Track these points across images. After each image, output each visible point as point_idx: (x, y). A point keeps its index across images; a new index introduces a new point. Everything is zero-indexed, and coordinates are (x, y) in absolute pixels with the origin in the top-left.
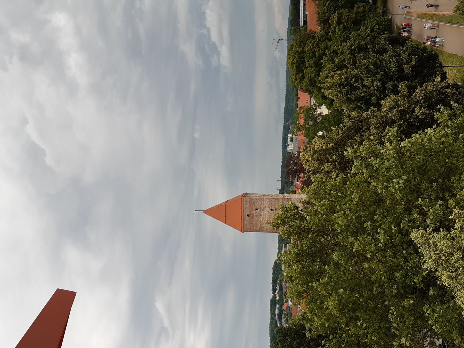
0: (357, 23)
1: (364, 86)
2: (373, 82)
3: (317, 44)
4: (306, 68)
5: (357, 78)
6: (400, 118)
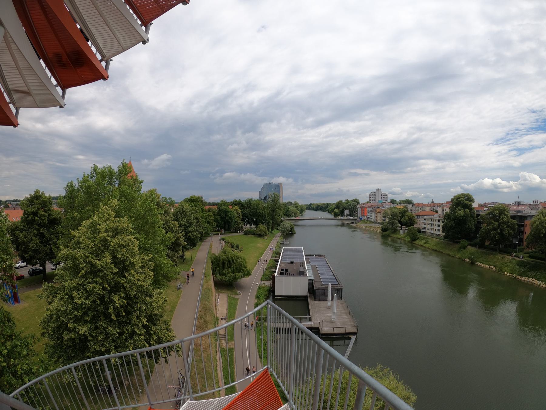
0: (208, 222)
1: (183, 218)
2: (184, 221)
3: (200, 207)
4: (191, 203)
5: (186, 215)
6: (169, 228)
